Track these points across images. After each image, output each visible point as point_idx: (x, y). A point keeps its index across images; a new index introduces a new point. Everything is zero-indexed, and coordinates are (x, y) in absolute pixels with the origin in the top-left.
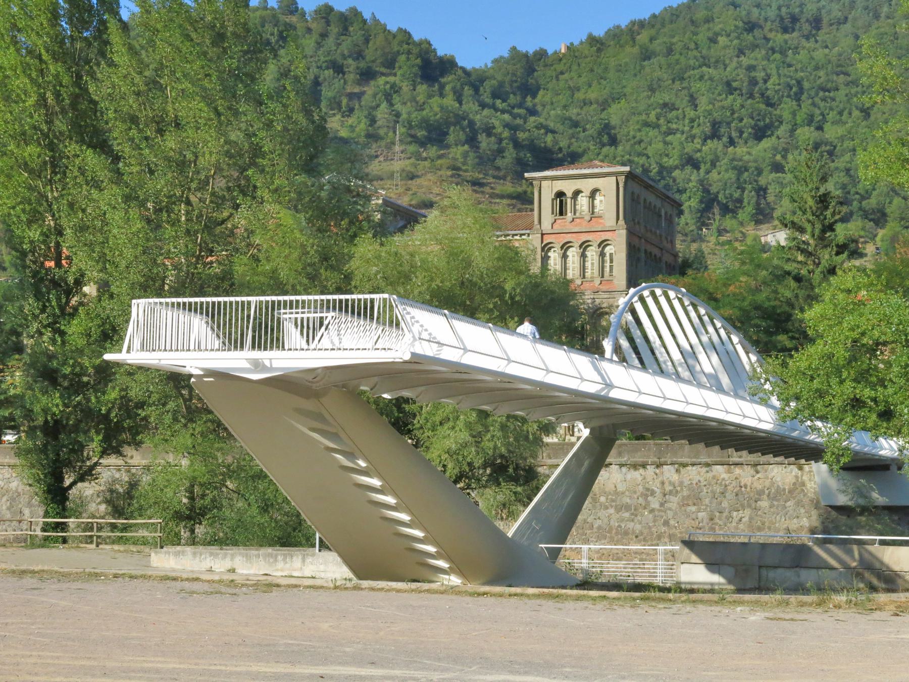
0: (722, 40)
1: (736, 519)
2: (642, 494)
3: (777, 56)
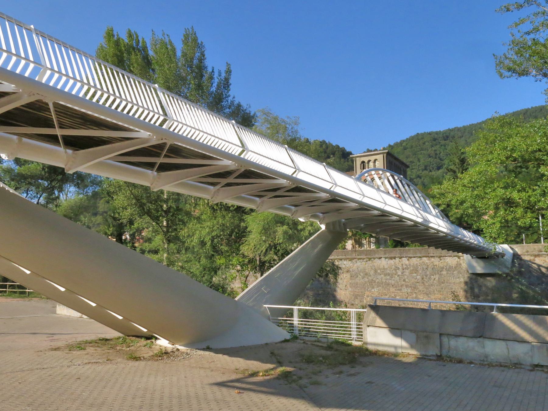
0: (427, 143)
1: (433, 279)
2: (394, 269)
3: (443, 147)
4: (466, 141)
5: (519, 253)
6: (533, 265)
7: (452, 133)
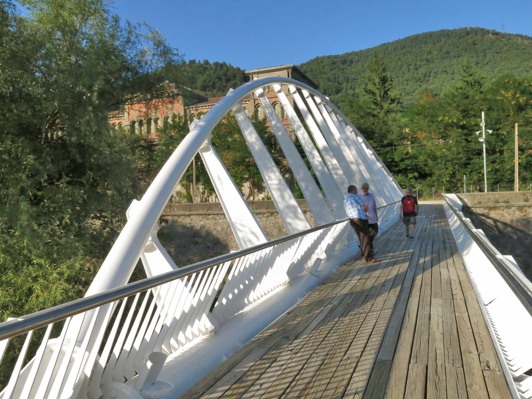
0: (326, 67)
3: (341, 71)
4: (363, 65)
5: (469, 204)
6: (488, 220)
7: (350, 58)
